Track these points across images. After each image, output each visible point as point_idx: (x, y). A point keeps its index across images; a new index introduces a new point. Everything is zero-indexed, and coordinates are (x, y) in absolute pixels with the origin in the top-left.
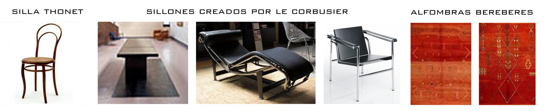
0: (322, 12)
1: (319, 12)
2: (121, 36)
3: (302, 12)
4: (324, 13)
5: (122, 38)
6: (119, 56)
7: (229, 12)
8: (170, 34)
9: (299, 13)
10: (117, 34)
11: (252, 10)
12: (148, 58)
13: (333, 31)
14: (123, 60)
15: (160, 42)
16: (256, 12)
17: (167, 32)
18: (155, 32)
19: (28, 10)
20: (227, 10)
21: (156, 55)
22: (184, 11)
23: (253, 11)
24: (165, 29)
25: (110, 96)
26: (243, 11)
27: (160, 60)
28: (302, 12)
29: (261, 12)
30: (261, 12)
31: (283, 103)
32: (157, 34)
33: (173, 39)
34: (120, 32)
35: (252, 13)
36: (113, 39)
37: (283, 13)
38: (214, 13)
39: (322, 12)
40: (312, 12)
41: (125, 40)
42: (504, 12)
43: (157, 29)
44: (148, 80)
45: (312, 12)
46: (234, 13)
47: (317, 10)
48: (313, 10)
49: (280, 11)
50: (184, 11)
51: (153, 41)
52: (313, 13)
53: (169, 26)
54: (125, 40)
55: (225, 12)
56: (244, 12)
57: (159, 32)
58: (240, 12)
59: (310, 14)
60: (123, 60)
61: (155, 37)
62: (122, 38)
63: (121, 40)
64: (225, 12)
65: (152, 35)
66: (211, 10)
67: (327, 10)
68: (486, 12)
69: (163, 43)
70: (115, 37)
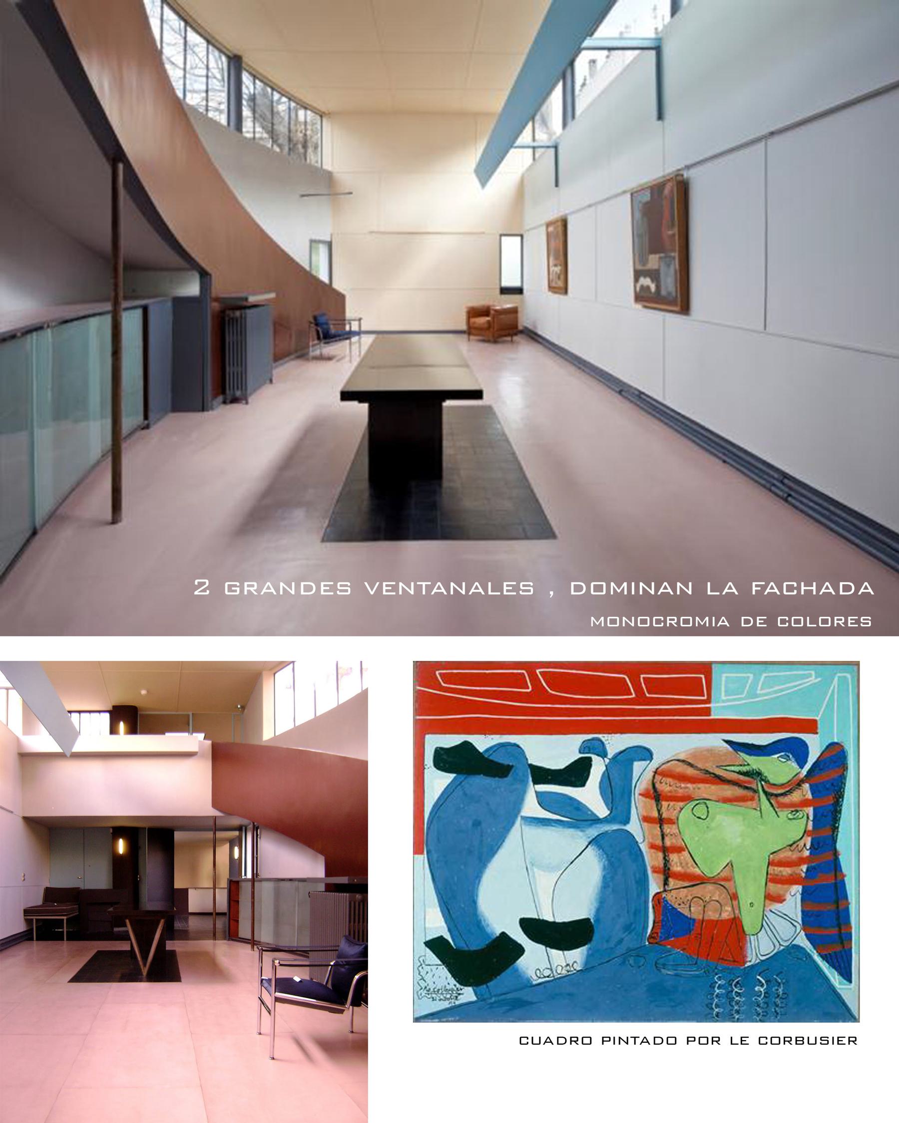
0: (812, 1041)
1: (806, 1041)
3: (775, 1041)
4: (816, 1044)
5: (358, 333)
9: (771, 1044)
11: (603, 1038)
13: (569, 291)
16: (610, 1041)
19: (731, 1038)
20: (558, 1038)
22: (840, 1039)
23: (690, 1039)
26: (823, 1039)
28: (775, 1041)
29: (703, 1041)
31: (436, 892)
35: (688, 1044)
36: (327, 337)
37: (741, 1044)
38: (796, 1044)
39: (812, 1041)
40: (793, 1041)
41: (367, 340)
42: (800, 1041)
45: (793, 1041)
46: (668, 1044)
47: (803, 1038)
48: (796, 1038)
49: (737, 1040)
50: (840, 1039)
52: (796, 1044)
54: (367, 340)
55: (555, 1041)
56: (761, 1041)
58: (580, 1040)
61: (471, 331)
62: (358, 333)
63: (355, 339)
64: (555, 1041)
66: (577, 1038)
67: (821, 1038)
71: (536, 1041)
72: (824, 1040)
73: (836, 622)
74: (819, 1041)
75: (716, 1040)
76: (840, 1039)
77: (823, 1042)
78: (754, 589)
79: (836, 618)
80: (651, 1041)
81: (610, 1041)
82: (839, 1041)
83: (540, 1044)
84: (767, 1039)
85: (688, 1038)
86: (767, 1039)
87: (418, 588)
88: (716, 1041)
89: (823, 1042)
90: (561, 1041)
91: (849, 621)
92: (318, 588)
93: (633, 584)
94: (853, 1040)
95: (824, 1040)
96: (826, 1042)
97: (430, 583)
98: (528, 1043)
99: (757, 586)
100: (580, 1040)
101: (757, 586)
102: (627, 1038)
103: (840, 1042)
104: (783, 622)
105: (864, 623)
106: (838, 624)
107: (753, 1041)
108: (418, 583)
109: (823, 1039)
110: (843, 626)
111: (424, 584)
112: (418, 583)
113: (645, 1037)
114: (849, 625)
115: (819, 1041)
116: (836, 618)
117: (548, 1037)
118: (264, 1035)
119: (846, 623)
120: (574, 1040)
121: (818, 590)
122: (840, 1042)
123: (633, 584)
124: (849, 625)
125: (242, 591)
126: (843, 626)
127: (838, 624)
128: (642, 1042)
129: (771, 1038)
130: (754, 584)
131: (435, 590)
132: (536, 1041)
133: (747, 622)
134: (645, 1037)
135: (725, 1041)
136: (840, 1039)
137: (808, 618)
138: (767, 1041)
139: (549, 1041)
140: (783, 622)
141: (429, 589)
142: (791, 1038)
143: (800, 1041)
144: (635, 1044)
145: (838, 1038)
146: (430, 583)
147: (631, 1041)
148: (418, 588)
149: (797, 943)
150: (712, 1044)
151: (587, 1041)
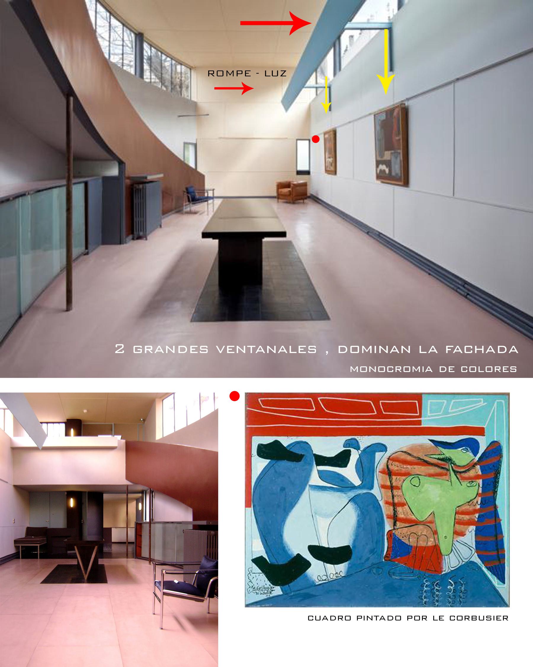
0: (481, 618)
1: (478, 618)
2: (210, 194)
3: (460, 618)
4: (484, 620)
5: (212, 198)
6: (205, 235)
7: (390, 618)
8: (311, 191)
9: (457, 620)
10: (203, 190)
12: (266, 240)
14: (214, 243)
15: (291, 206)
16: (361, 618)
17: (305, 185)
18: (281, 186)
19: (434, 616)
21: (283, 234)
23: (409, 617)
24: (301, 180)
25: (188, 319)
26: (488, 617)
27: (290, 243)
29: (417, 618)
30: (417, 618)
32: (286, 190)
33: (316, 200)
34: (207, 186)
36: (194, 200)
37: (440, 620)
38: (472, 620)
39: (481, 618)
40: (470, 619)
41: (218, 202)
42: (474, 618)
43: (284, 179)
44: (264, 287)
45: (470, 619)
47: (476, 616)
48: (472, 616)
49: (437, 618)
51: (276, 206)
52: (472, 620)
53: (308, 173)
54: (218, 202)
55: (329, 618)
57: (287, 185)
59: (213, 76)
60: (214, 243)
61: (279, 197)
62: (212, 198)
63: (210, 201)
64: (329, 618)
65: (275, 194)
67: (487, 616)
68: (393, 10)
69: (297, 209)
70: (197, 196)
71: (318, 618)
72: (489, 618)
73: (496, 369)
74: (485, 618)
75: (425, 618)
76: (498, 617)
77: (488, 619)
78: (447, 350)
79: (495, 367)
80: (386, 618)
81: (361, 618)
82: (497, 618)
83: (320, 620)
84: (455, 617)
85: (408, 616)
86: (455, 617)
87: (248, 349)
88: (425, 619)
89: (488, 619)
90: (333, 618)
91: (504, 369)
92: (189, 350)
93: (375, 347)
94: (506, 618)
95: (489, 618)
96: (490, 619)
97: (255, 346)
98: (313, 619)
99: (449, 348)
100: (344, 618)
101: (449, 348)
102: (372, 616)
103: (498, 619)
104: (464, 369)
105: (512, 370)
106: (497, 370)
107: (446, 618)
108: (248, 346)
109: (488, 617)
110: (500, 372)
111: (251, 347)
112: (248, 346)
113: (382, 616)
114: (504, 371)
115: (485, 618)
116: (495, 367)
117: (325, 616)
118: (156, 614)
119: (501, 370)
120: (340, 618)
121: (485, 350)
122: (498, 619)
123: (375, 347)
124: (504, 371)
125: (143, 351)
126: (500, 372)
127: (497, 370)
128: (381, 619)
129: (457, 616)
130: (447, 347)
131: (258, 351)
132: (318, 618)
133: (443, 369)
134: (382, 616)
135: (430, 618)
136: (498, 617)
137: (479, 367)
138: (455, 618)
139: (325, 618)
140: (464, 369)
141: (254, 350)
142: (469, 616)
143: (474, 618)
144: (376, 620)
145: (497, 616)
146: (255, 346)
147: (374, 618)
148: (248, 349)
149: (473, 560)
150: (422, 620)
151: (348, 618)
